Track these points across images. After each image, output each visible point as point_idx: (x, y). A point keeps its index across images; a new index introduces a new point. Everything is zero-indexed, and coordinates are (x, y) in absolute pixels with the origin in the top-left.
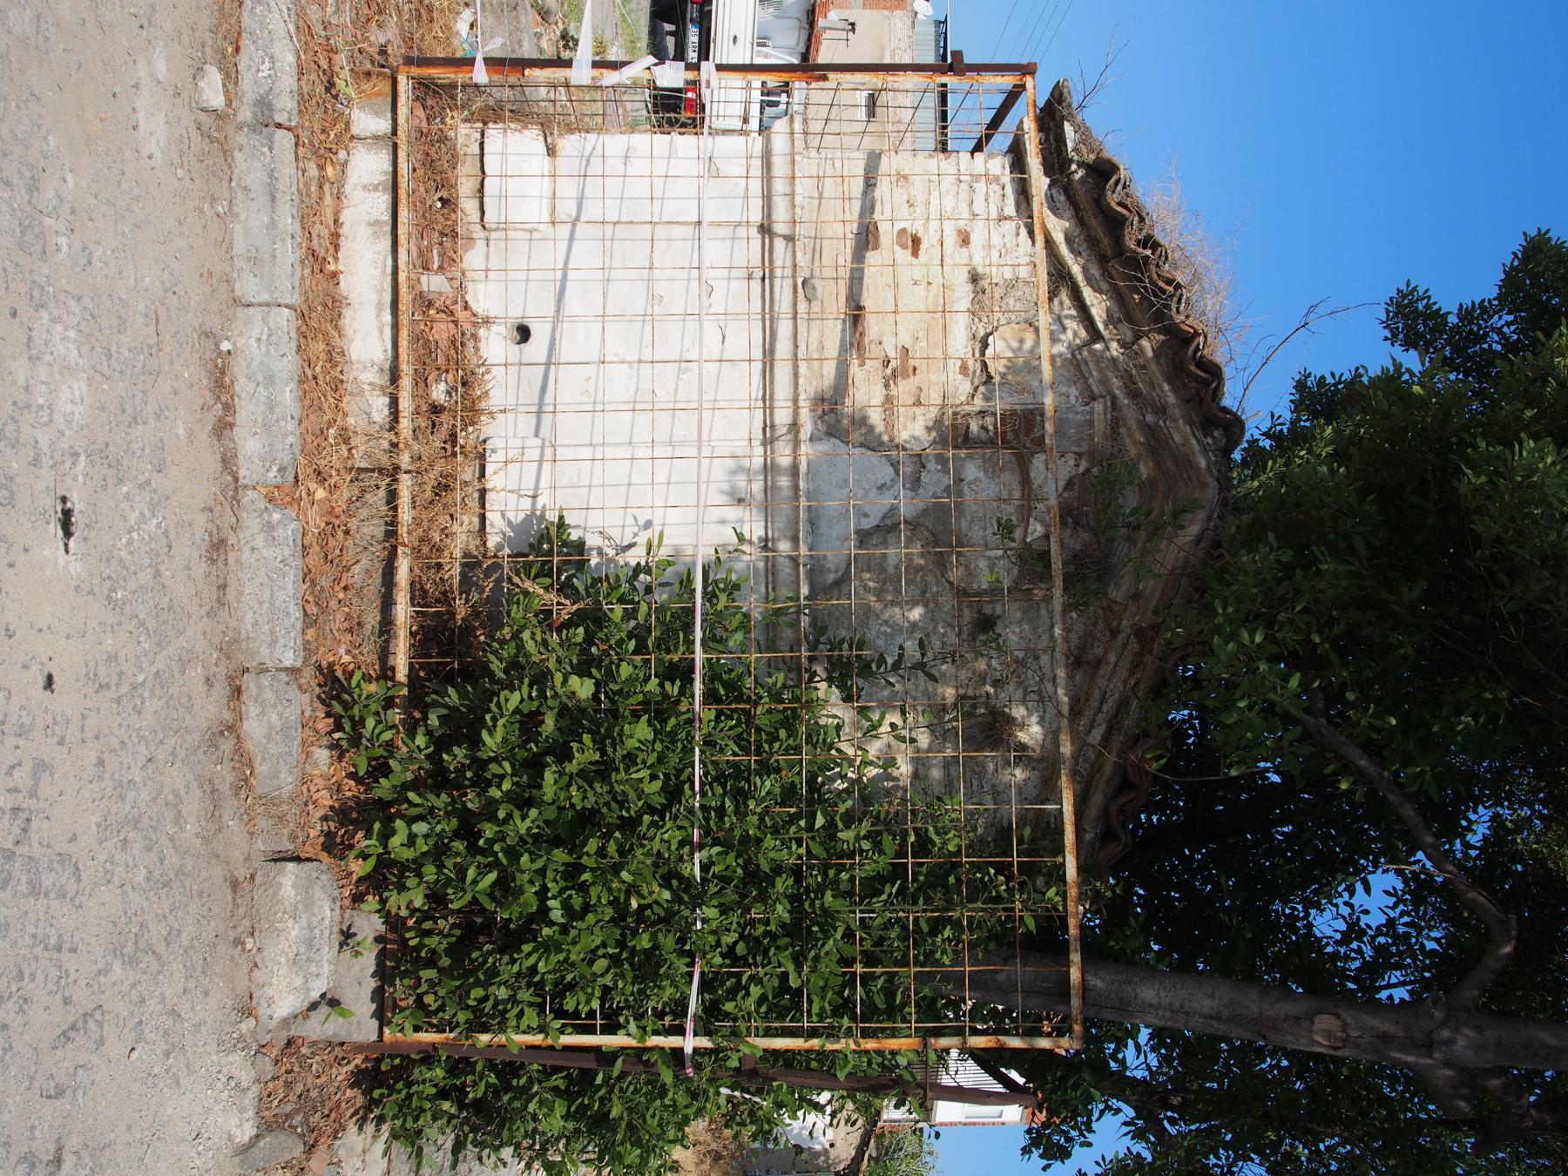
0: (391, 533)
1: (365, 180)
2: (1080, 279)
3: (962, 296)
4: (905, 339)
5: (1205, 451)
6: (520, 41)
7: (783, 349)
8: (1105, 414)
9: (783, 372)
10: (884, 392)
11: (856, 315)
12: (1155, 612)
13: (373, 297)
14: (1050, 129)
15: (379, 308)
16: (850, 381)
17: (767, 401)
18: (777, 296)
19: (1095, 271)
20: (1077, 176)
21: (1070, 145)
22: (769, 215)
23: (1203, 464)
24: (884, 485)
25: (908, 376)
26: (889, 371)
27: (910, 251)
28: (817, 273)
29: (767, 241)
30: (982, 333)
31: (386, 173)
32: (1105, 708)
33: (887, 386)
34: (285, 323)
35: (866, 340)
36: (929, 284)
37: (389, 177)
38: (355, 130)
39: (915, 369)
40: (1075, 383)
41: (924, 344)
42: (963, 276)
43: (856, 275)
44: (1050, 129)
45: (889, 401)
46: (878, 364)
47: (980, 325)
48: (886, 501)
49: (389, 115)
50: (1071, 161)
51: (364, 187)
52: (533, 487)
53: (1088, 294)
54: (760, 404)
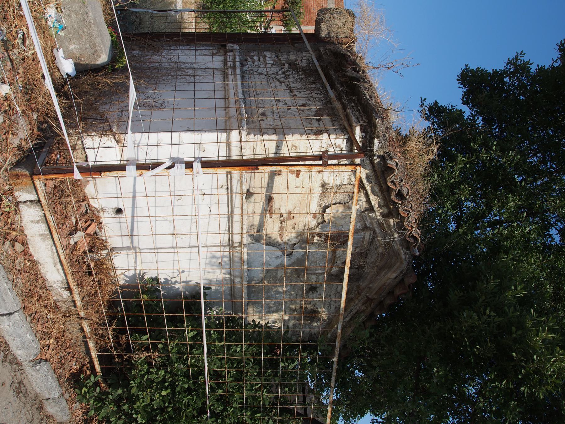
0: (85, 337)
1: (31, 219)
2: (369, 192)
3: (318, 189)
4: (290, 208)
5: (405, 254)
6: (87, 13)
7: (237, 211)
8: (370, 236)
9: (237, 218)
10: (280, 225)
11: (269, 199)
12: (375, 294)
13: (51, 260)
14: (368, 132)
15: (55, 264)
16: (266, 222)
17: (230, 231)
18: (234, 199)
19: (377, 189)
20: (376, 162)
21: (376, 148)
22: (229, 153)
23: (404, 257)
24: (278, 257)
25: (290, 219)
26: (282, 218)
27: (295, 175)
28: (252, 186)
29: (229, 176)
30: (324, 205)
31: (41, 216)
32: (351, 313)
33: (281, 223)
34: (18, 318)
35: (273, 209)
36: (303, 187)
37: (43, 218)
38: (19, 200)
39: (293, 217)
40: (360, 222)
41: (299, 208)
42: (319, 184)
43: (270, 185)
44: (368, 132)
45: (281, 228)
46: (278, 216)
47: (323, 202)
48: (278, 261)
49: (35, 193)
50: (375, 155)
51: (32, 222)
52: (132, 191)
53: (372, 197)
54: (227, 232)
